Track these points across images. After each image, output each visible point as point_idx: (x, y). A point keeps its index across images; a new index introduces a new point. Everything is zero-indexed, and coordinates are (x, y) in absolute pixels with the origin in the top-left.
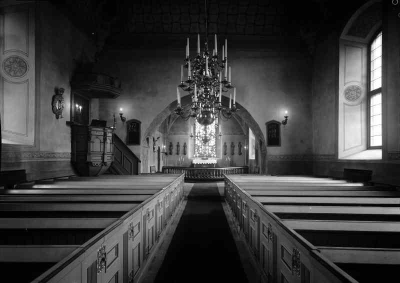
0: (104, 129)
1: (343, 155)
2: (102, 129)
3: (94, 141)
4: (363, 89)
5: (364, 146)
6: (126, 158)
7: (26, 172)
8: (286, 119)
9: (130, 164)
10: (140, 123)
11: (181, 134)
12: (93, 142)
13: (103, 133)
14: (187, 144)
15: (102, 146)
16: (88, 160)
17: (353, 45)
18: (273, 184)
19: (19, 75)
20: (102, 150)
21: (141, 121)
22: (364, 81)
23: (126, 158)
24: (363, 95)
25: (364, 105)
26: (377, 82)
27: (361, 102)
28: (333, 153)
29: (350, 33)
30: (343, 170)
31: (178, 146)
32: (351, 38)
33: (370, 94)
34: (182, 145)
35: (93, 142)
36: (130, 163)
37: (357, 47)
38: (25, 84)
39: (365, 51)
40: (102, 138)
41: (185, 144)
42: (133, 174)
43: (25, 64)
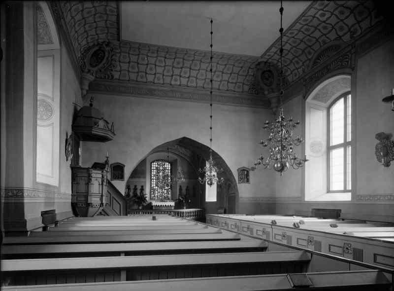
0: (102, 172)
1: (308, 198)
2: (100, 172)
3: (94, 183)
4: (324, 144)
5: (325, 191)
6: (115, 200)
7: (56, 212)
8: (108, 159)
9: (119, 205)
10: (124, 166)
11: (139, 177)
12: (93, 184)
13: (101, 175)
14: (144, 188)
15: (101, 189)
16: (89, 202)
17: (317, 108)
18: (88, 233)
19: (45, 118)
20: (101, 192)
21: (125, 165)
22: (325, 138)
23: (115, 200)
24: (324, 148)
25: (325, 157)
26: (338, 137)
27: (323, 155)
28: (300, 195)
29: (315, 98)
30: (311, 210)
31: (135, 189)
32: (315, 102)
33: (329, 148)
34: (139, 188)
35: (93, 184)
36: (119, 204)
37: (318, 109)
38: (51, 128)
39: (325, 113)
40: (100, 180)
41: (142, 187)
42: (124, 215)
43: (50, 108)
